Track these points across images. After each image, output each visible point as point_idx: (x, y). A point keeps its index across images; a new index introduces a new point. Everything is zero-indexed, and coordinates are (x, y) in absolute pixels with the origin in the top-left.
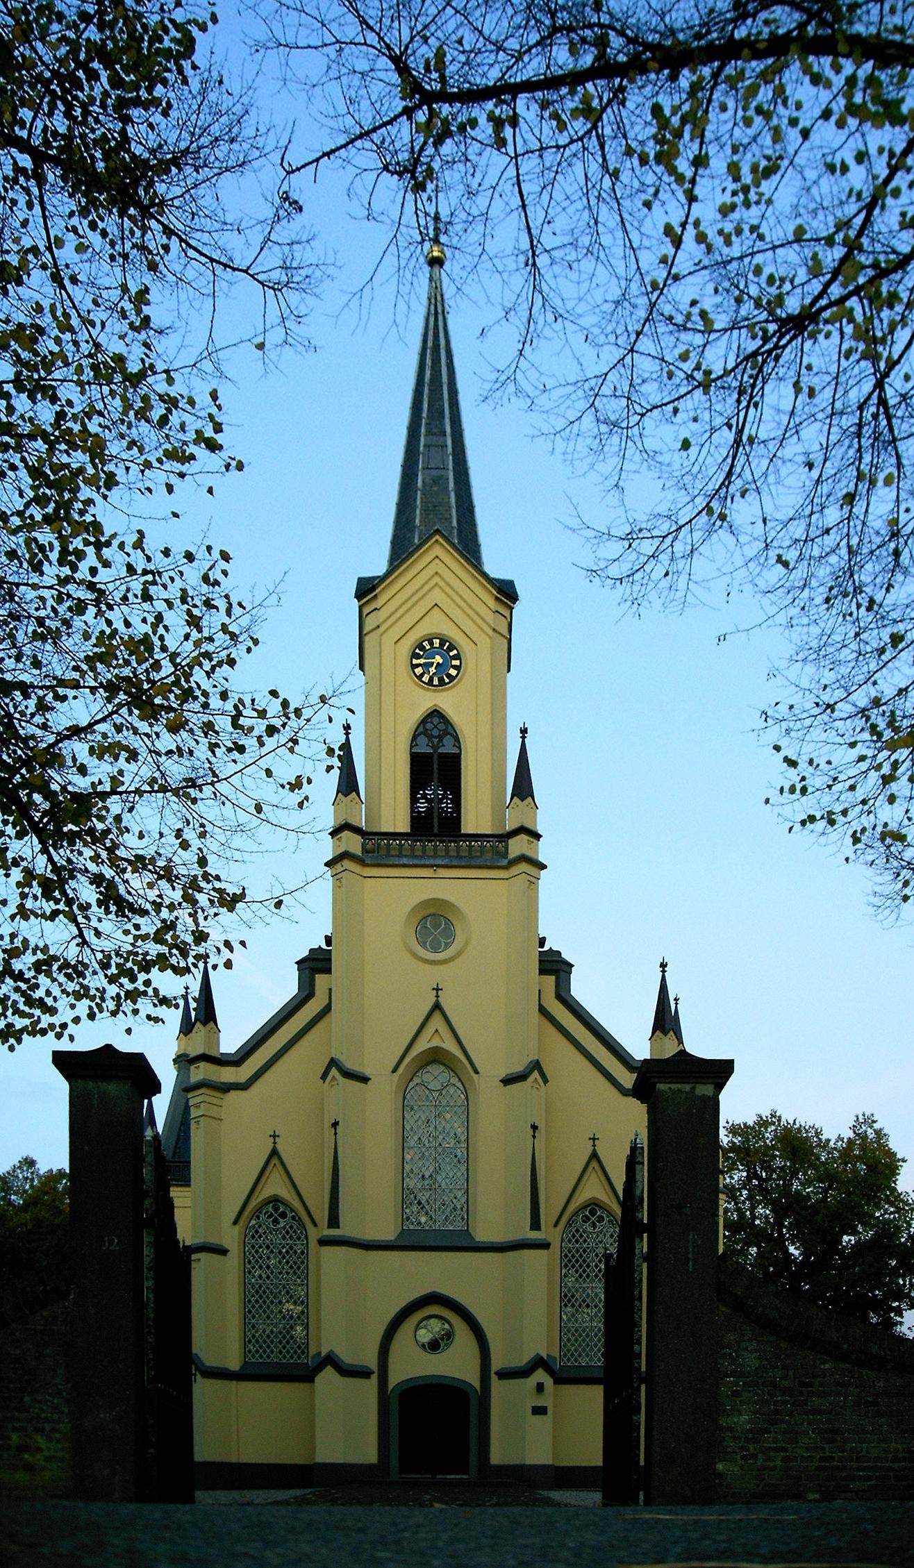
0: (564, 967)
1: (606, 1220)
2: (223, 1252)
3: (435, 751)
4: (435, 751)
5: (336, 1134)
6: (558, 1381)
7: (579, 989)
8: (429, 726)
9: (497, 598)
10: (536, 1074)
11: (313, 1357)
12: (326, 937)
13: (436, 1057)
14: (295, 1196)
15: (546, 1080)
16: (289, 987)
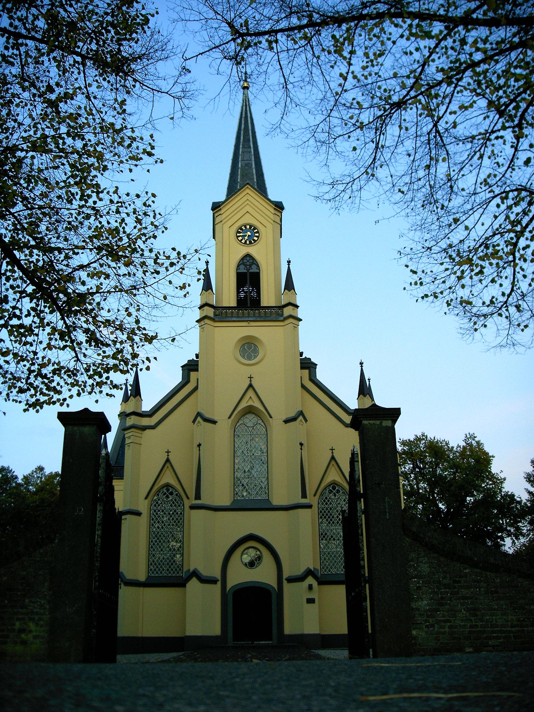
0: (313, 366)
1: (341, 492)
2: (139, 514)
3: (248, 271)
4: (248, 271)
5: (199, 450)
6: (320, 583)
7: (320, 376)
8: (245, 261)
9: (275, 209)
10: (301, 418)
11: (185, 572)
12: (196, 354)
13: (250, 410)
14: (178, 483)
15: (306, 420)
16: (178, 378)
